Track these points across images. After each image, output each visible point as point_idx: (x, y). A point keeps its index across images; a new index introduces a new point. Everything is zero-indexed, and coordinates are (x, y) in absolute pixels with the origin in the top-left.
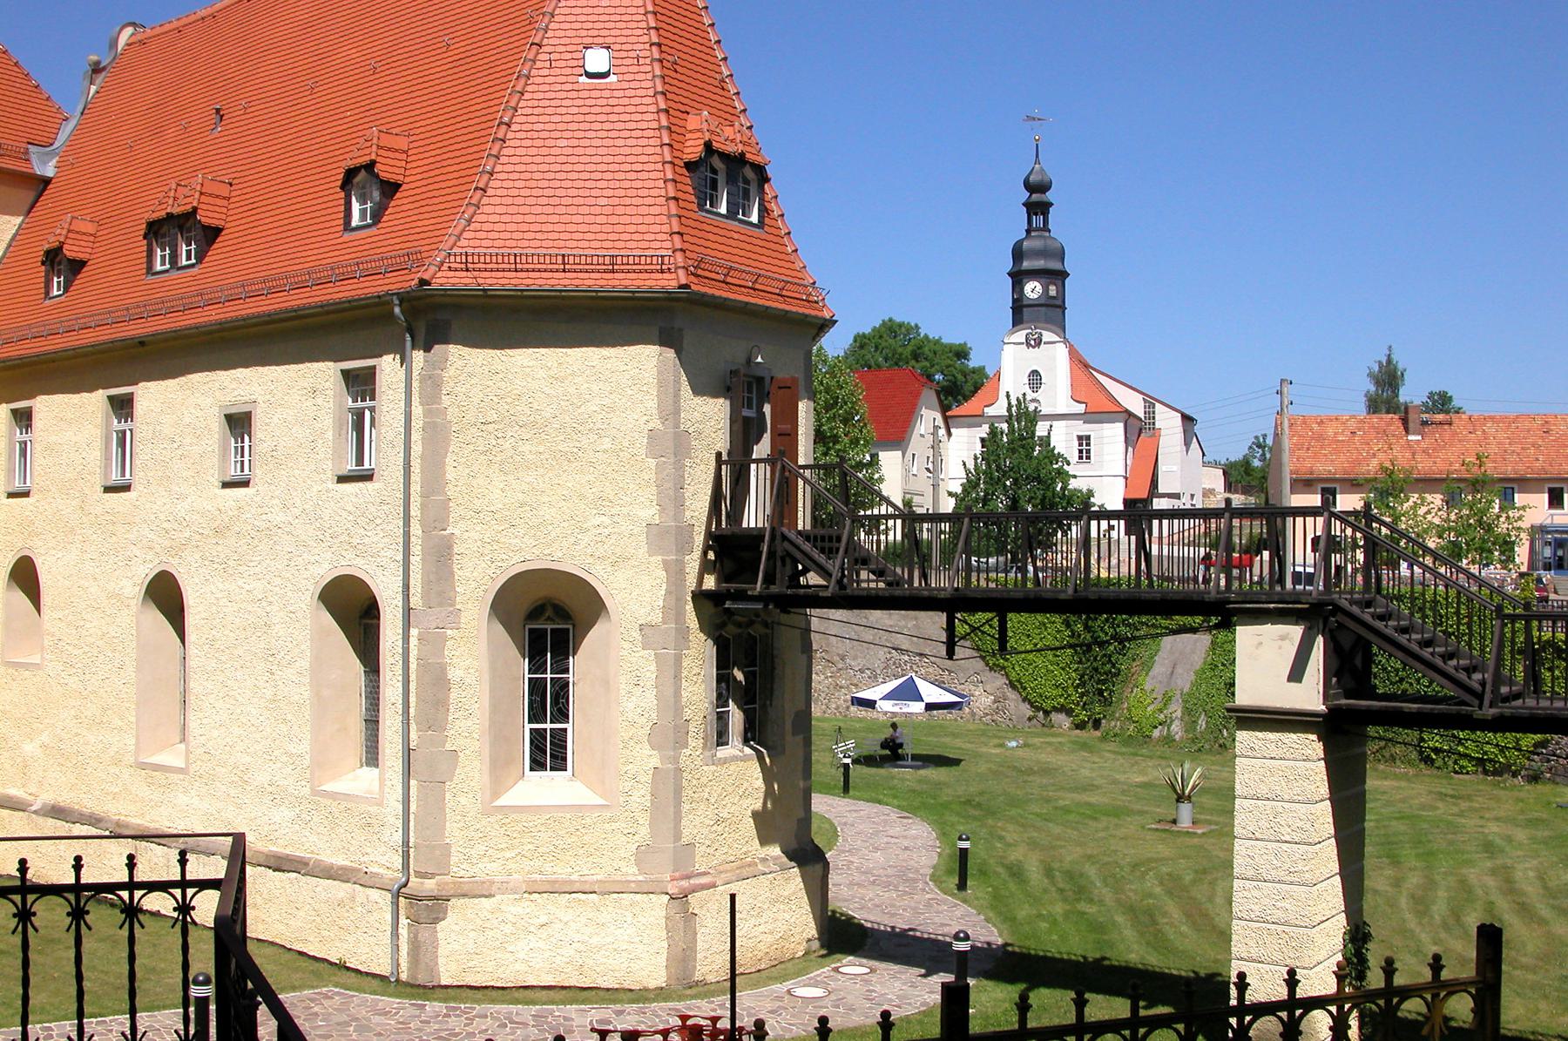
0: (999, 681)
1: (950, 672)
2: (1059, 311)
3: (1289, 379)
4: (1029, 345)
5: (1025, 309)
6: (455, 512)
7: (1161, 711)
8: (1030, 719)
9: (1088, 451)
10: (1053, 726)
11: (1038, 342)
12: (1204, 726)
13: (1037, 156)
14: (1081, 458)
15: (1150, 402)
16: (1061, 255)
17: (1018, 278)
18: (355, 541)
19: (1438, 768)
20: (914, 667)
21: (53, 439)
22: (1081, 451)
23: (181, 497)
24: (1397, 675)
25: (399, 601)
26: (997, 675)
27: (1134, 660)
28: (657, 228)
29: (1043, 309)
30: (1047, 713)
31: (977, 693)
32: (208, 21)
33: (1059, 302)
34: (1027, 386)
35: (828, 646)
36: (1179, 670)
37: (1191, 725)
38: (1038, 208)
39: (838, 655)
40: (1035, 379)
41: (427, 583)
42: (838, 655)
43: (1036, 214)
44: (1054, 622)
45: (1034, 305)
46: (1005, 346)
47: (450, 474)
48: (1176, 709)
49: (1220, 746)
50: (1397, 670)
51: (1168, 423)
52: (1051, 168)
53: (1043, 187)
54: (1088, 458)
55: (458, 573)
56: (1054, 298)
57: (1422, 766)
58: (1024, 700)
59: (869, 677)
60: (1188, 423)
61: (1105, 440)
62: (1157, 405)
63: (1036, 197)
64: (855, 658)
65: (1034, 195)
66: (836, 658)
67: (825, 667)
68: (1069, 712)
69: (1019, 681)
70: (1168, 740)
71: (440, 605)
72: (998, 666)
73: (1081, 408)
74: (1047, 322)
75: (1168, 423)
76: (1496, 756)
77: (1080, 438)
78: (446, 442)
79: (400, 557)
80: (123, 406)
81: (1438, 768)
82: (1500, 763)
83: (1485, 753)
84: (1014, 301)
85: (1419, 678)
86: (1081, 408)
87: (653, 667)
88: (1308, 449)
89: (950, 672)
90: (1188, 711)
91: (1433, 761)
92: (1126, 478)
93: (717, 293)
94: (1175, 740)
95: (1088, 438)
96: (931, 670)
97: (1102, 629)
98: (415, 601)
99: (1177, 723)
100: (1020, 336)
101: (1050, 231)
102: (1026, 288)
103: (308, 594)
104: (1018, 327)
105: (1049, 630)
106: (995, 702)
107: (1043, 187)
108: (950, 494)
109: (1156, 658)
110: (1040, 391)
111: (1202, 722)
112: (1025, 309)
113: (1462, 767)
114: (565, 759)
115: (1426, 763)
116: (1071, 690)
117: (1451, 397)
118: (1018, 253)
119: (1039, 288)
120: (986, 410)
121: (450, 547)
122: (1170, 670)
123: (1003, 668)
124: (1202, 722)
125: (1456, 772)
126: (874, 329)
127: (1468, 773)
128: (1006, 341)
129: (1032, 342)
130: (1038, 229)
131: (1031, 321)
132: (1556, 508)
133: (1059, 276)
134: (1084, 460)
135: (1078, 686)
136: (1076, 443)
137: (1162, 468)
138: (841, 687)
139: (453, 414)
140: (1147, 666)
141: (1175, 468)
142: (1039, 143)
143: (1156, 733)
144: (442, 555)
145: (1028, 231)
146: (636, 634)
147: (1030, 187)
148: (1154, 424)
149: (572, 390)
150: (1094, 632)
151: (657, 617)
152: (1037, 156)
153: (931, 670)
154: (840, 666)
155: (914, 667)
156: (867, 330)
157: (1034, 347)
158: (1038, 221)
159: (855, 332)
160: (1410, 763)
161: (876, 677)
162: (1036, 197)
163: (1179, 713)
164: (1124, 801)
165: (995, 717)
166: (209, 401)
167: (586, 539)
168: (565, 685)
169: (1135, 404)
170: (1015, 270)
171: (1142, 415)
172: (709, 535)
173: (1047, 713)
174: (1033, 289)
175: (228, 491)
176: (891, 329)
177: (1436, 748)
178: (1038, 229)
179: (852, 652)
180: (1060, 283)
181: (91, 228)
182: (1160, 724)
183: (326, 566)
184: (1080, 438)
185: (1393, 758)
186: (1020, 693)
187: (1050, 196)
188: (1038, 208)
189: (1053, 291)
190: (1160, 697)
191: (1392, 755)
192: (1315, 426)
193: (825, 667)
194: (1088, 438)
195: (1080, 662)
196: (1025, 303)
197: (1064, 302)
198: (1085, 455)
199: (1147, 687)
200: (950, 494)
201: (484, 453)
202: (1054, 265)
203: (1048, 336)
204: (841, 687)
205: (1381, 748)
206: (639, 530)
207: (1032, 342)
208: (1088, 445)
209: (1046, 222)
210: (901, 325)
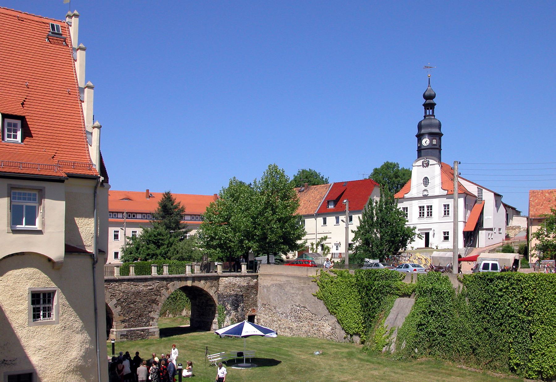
0: (334, 319)
1: (315, 315)
2: (438, 150)
3: (459, 161)
4: (423, 166)
5: (422, 151)
7: (388, 337)
8: (345, 338)
9: (431, 212)
10: (353, 342)
11: (428, 165)
12: (404, 346)
13: (429, 83)
14: (445, 214)
15: (480, 188)
16: (439, 126)
17: (420, 137)
19: (518, 375)
20: (302, 312)
22: (445, 211)
24: (499, 322)
26: (333, 317)
27: (382, 311)
29: (430, 150)
30: (351, 336)
31: (325, 325)
33: (438, 147)
34: (423, 184)
35: (270, 303)
36: (399, 317)
37: (398, 347)
38: (429, 106)
39: (273, 306)
40: (426, 181)
42: (273, 306)
43: (428, 109)
44: (354, 292)
45: (426, 148)
46: (414, 168)
48: (394, 337)
49: (412, 357)
50: (499, 319)
51: (488, 198)
52: (435, 89)
53: (432, 97)
56: (434, 145)
57: (510, 373)
58: (343, 329)
59: (285, 317)
60: (498, 198)
61: (413, 205)
62: (483, 190)
63: (428, 101)
64: (279, 308)
65: (427, 101)
66: (273, 308)
67: (269, 312)
68: (360, 335)
69: (340, 320)
70: (388, 353)
72: (333, 312)
73: (445, 193)
74: (431, 156)
75: (488, 198)
76: (548, 370)
77: (445, 206)
81: (518, 375)
82: (551, 374)
83: (542, 368)
84: (419, 147)
85: (510, 324)
86: (445, 193)
88: (542, 205)
89: (315, 315)
90: (399, 339)
91: (515, 371)
92: (465, 222)
94: (391, 353)
96: (308, 314)
97: (372, 295)
99: (393, 344)
100: (420, 163)
101: (434, 116)
102: (423, 141)
104: (420, 158)
105: (353, 296)
106: (332, 329)
107: (432, 97)
108: (352, 231)
109: (391, 310)
110: (428, 186)
111: (404, 345)
112: (422, 151)
113: (529, 375)
115: (512, 371)
116: (360, 325)
118: (420, 127)
120: (405, 195)
122: (395, 316)
123: (335, 314)
124: (404, 345)
125: (527, 378)
126: (382, 167)
127: (533, 379)
128: (414, 165)
129: (425, 165)
130: (429, 115)
131: (424, 156)
132: (34, 201)
133: (439, 135)
134: (447, 215)
135: (363, 323)
136: (443, 208)
137: (485, 217)
138: (275, 321)
140: (386, 316)
141: (491, 217)
142: (430, 78)
143: (384, 349)
145: (425, 117)
147: (426, 97)
148: (482, 198)
150: (369, 296)
152: (429, 83)
153: (308, 314)
154: (274, 311)
155: (302, 312)
156: (379, 167)
157: (426, 167)
158: (429, 112)
159: (375, 167)
160: (504, 370)
161: (287, 317)
162: (428, 101)
163: (395, 339)
164: (454, 367)
165: (332, 337)
169: (473, 189)
170: (419, 134)
171: (477, 195)
173: (351, 336)
174: (426, 142)
175: (330, 242)
177: (517, 363)
178: (429, 115)
179: (278, 305)
180: (438, 138)
182: (386, 345)
184: (445, 206)
185: (495, 368)
186: (341, 325)
187: (435, 101)
188: (429, 106)
189: (434, 142)
190: (389, 330)
191: (495, 366)
192: (547, 195)
193: (269, 312)
195: (364, 311)
196: (422, 148)
197: (440, 146)
199: (385, 325)
200: (352, 231)
202: (437, 131)
203: (431, 162)
204: (275, 321)
205: (489, 362)
207: (425, 165)
208: (448, 208)
209: (433, 112)
210: (391, 164)
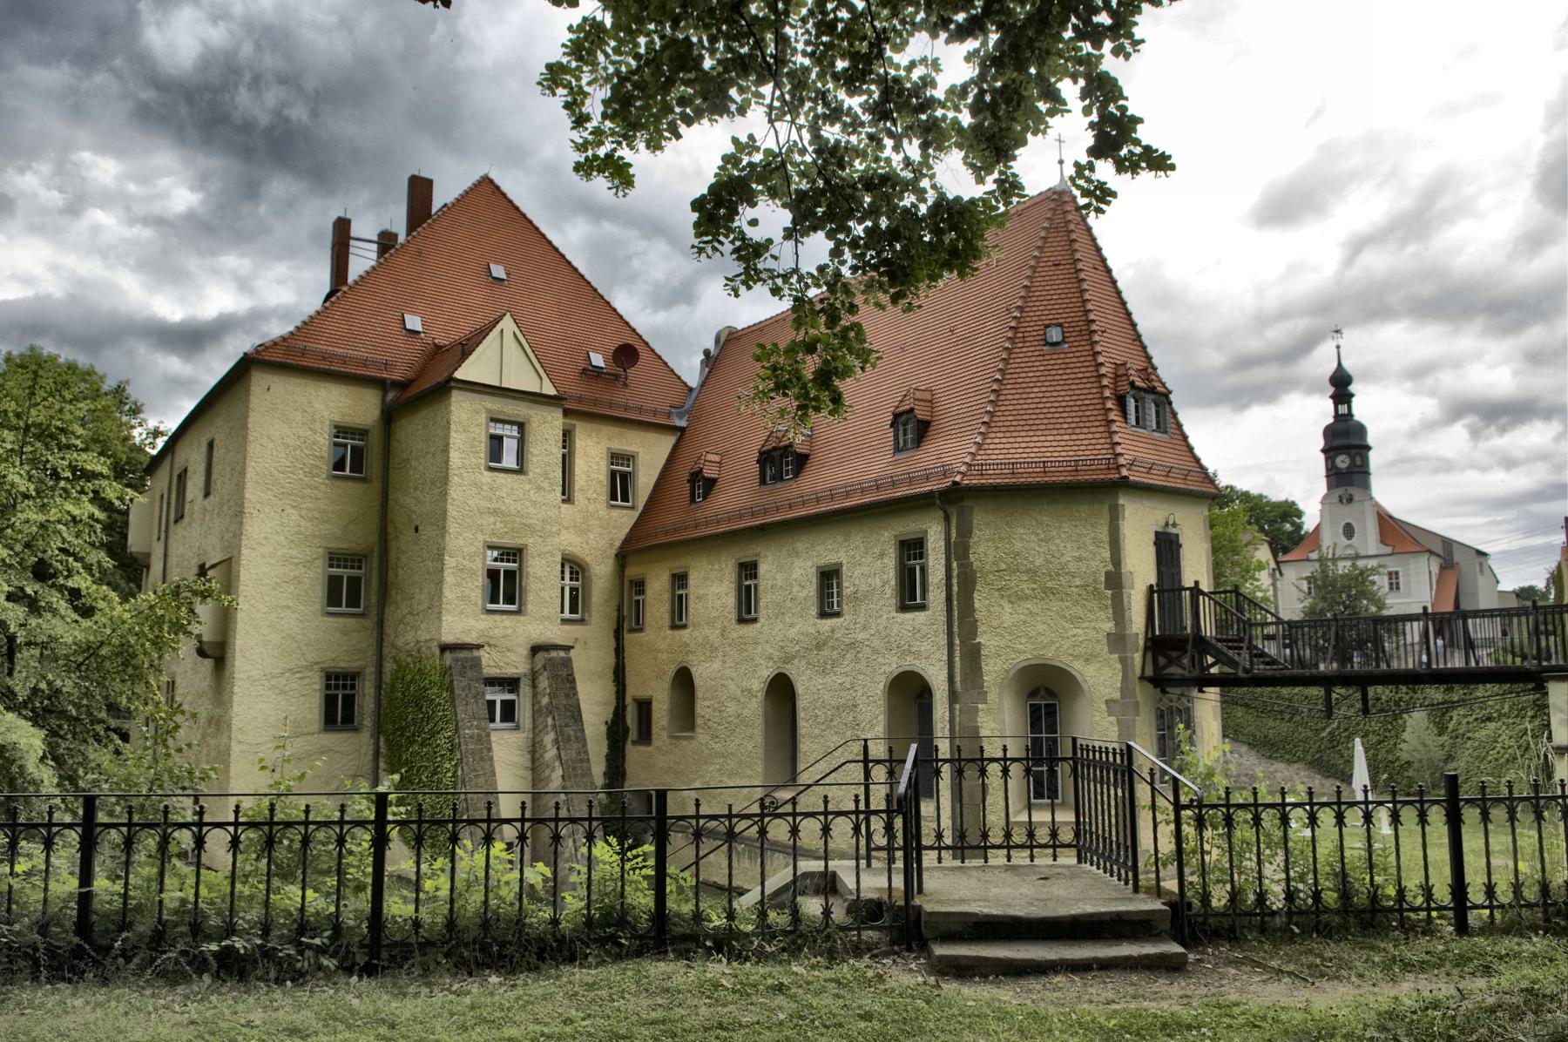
6: (981, 628)
9: (1398, 584)
14: (1391, 588)
18: (913, 649)
21: (702, 592)
22: (1391, 584)
23: (792, 625)
25: (945, 686)
28: (1103, 441)
32: (781, 323)
41: (964, 676)
47: (977, 605)
54: (1398, 588)
55: (985, 668)
71: (974, 688)
78: (974, 583)
79: (945, 658)
80: (748, 570)
86: (1388, 550)
87: (1116, 729)
93: (1146, 481)
95: (1397, 573)
98: (958, 685)
103: (881, 686)
114: (1057, 791)
117: (661, 148)
119: (1348, 461)
121: (979, 651)
139: (976, 565)
144: (973, 655)
146: (1104, 707)
149: (1054, 548)
151: (1117, 695)
166: (809, 564)
167: (1067, 644)
168: (1055, 741)
172: (1146, 639)
176: (1293, 503)
181: (716, 458)
183: (895, 666)
194: (1397, 573)
198: (1394, 586)
201: (998, 590)
206: (1102, 637)
209: (1350, 408)
